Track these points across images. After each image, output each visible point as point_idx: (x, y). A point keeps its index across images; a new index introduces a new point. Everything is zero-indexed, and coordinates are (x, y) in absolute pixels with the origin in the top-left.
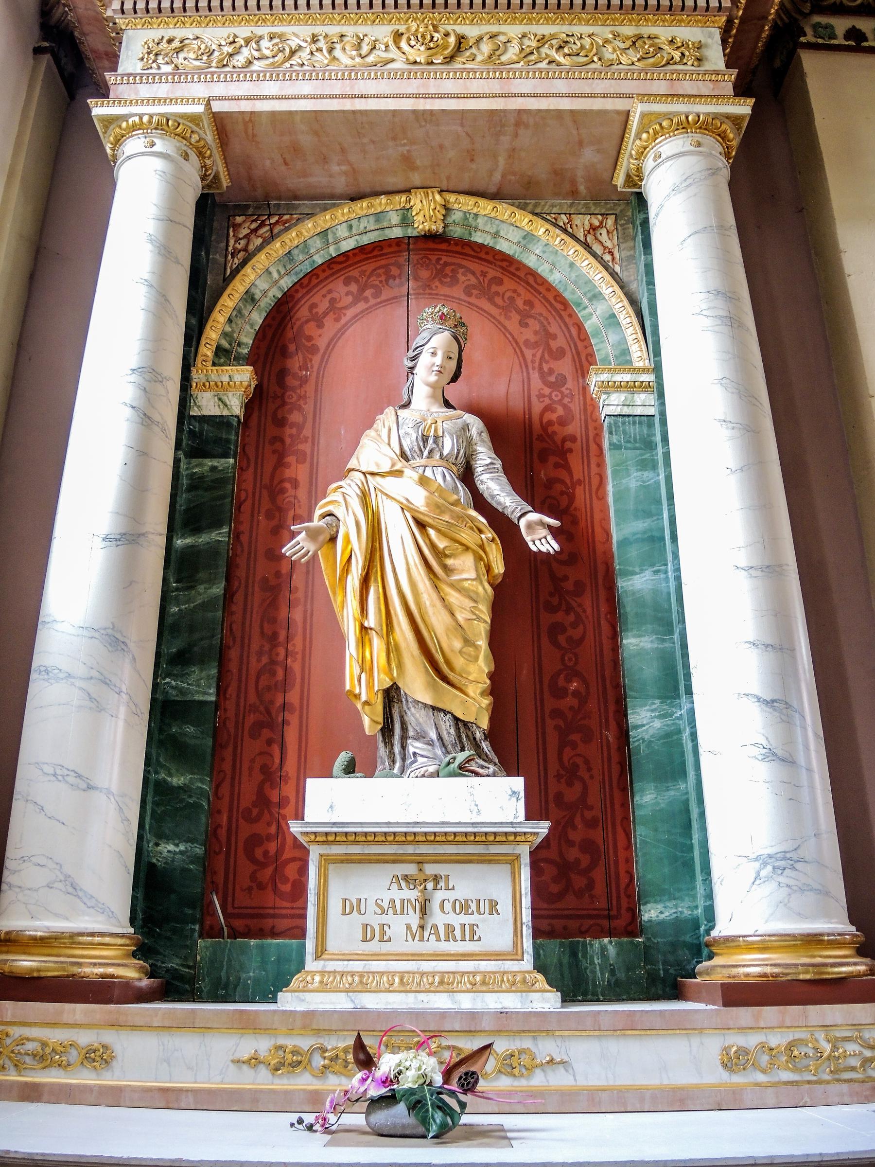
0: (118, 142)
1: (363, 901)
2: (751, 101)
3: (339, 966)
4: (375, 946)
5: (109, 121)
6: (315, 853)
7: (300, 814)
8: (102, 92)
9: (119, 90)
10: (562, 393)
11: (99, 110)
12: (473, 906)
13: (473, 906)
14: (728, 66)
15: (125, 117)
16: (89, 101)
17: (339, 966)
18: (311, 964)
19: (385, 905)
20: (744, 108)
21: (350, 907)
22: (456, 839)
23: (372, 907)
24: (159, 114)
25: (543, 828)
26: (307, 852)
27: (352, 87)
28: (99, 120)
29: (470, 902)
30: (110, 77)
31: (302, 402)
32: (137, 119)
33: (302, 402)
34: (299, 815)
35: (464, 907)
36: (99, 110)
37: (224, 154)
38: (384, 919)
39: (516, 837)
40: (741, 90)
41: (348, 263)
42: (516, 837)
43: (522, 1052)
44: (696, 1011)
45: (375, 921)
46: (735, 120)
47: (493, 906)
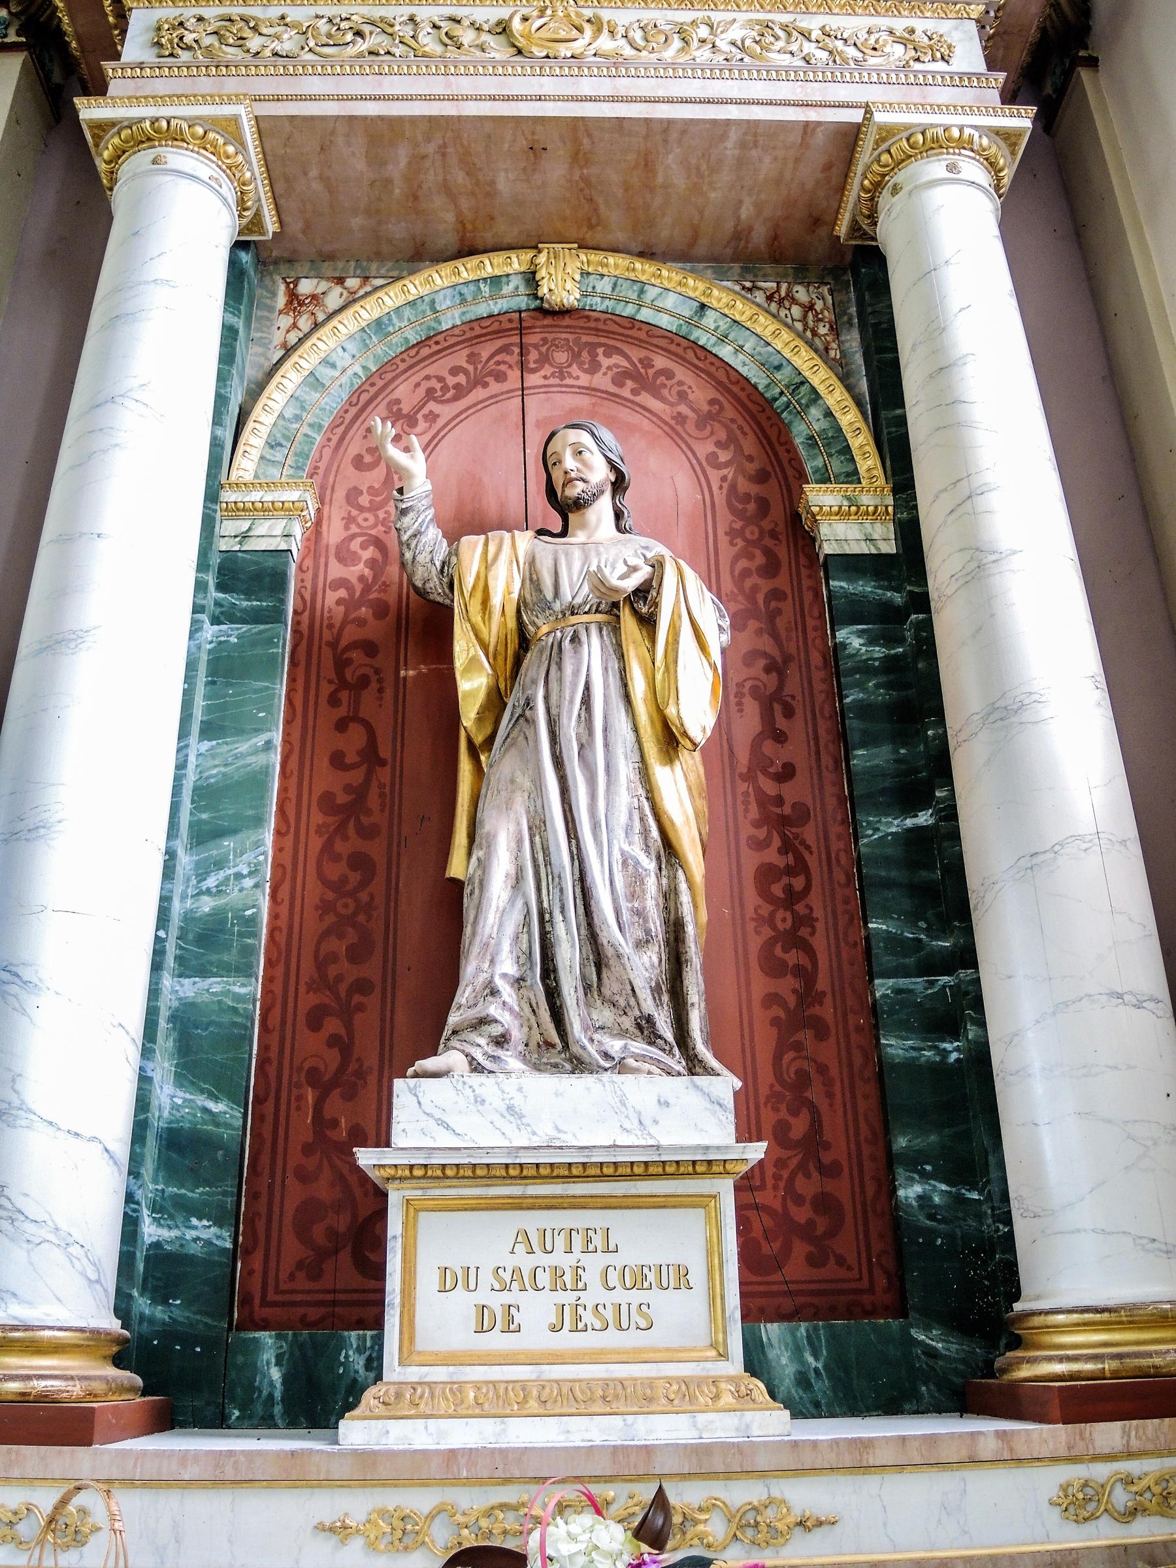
0: (119, 155)
1: (472, 1272)
2: (1032, 110)
3: (439, 1374)
4: (496, 1341)
5: (102, 128)
6: (395, 1198)
7: (383, 1138)
8: (97, 87)
9: (114, 88)
10: (377, 517)
11: (89, 110)
12: (651, 1277)
13: (651, 1277)
14: (991, 64)
15: (131, 124)
16: (76, 100)
17: (439, 1374)
18: (393, 1370)
19: (507, 1277)
20: (1021, 120)
21: (448, 1281)
22: (586, 1174)
23: (487, 1278)
24: (971, 126)
25: (756, 1151)
26: (384, 1195)
27: (449, 85)
28: (90, 127)
29: (646, 1270)
30: (108, 66)
31: (738, 525)
32: (940, 131)
33: (738, 525)
34: (383, 1139)
35: (638, 1279)
36: (89, 110)
37: (845, 182)
38: (506, 1298)
39: (616, 1169)
40: (1010, 96)
41: (626, 332)
42: (616, 1169)
43: (770, 1502)
44: (311, 1451)
45: (497, 1301)
46: (1007, 137)
47: (682, 1273)
